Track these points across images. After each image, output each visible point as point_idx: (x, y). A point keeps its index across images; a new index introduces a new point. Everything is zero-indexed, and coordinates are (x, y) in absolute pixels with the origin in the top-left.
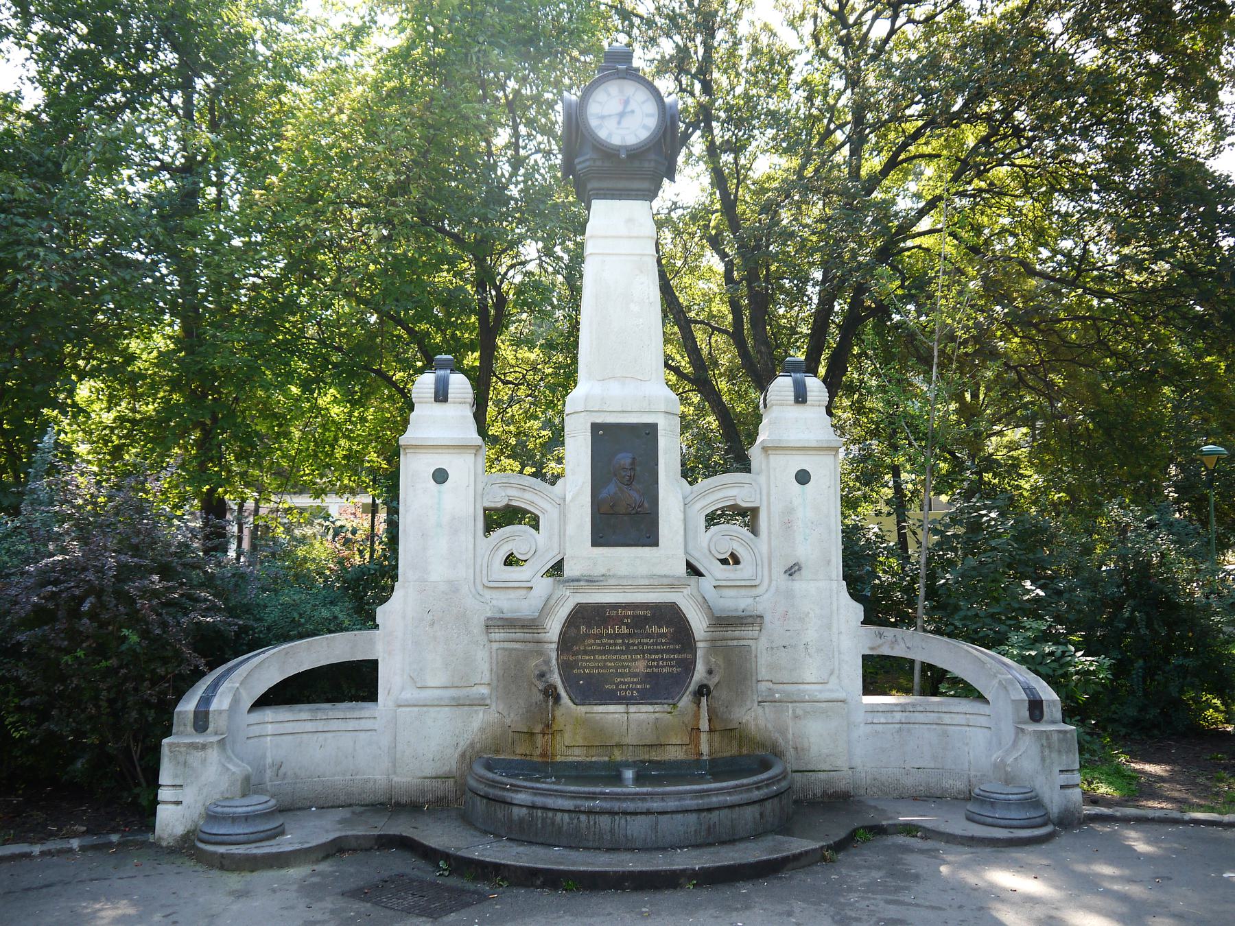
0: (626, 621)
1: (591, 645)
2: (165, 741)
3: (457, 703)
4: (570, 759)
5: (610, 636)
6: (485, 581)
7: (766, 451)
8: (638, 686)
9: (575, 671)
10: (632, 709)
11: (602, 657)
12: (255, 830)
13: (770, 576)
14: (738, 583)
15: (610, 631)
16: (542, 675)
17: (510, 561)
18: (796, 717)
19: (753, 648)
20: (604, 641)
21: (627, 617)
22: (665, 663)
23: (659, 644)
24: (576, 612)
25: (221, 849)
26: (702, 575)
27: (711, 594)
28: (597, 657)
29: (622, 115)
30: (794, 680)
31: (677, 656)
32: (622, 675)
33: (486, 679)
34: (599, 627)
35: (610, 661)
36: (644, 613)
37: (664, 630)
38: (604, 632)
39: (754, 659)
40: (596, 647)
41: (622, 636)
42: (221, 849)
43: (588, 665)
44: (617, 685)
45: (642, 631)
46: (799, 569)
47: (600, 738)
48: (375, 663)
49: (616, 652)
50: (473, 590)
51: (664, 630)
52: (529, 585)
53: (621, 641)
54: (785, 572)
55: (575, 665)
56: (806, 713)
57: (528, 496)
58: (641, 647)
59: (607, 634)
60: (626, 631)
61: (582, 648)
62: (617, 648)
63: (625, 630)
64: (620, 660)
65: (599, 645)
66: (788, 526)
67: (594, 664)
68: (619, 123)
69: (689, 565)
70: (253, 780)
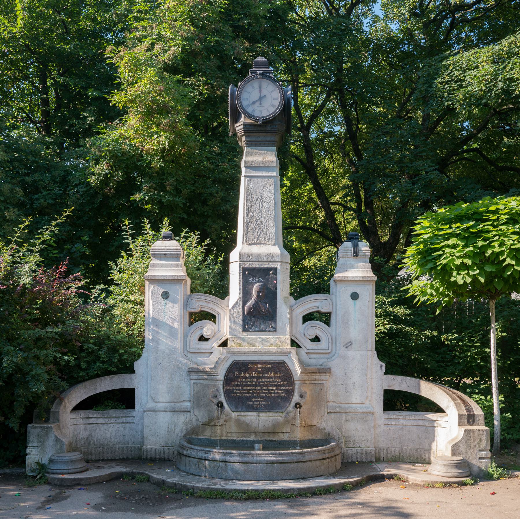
0: (258, 370)
1: (240, 382)
2: (29, 425)
3: (174, 411)
4: (230, 438)
5: (250, 377)
6: (188, 349)
7: (336, 282)
8: (264, 403)
9: (233, 395)
10: (261, 414)
11: (246, 388)
12: (74, 467)
13: (336, 348)
14: (319, 351)
15: (250, 375)
16: (216, 396)
17: (202, 339)
18: (347, 420)
19: (325, 385)
20: (247, 380)
21: (260, 368)
22: (278, 391)
23: (275, 382)
24: (233, 365)
25: (61, 476)
26: (300, 347)
27: (305, 357)
28: (243, 388)
29: (261, 99)
30: (346, 402)
31: (284, 388)
32: (256, 397)
33: (186, 397)
34: (245, 373)
35: (250, 390)
36: (268, 366)
37: (278, 375)
38: (247, 375)
39: (325, 390)
40: (243, 383)
41: (257, 378)
42: (61, 476)
43: (240, 392)
44: (254, 402)
45: (267, 375)
46: (351, 344)
47: (246, 429)
48: (133, 390)
49: (253, 386)
50: (183, 354)
51: (278, 375)
52: (211, 351)
53: (255, 380)
54: (344, 346)
55: (232, 391)
56: (353, 418)
57: (211, 305)
58: (266, 383)
59: (249, 376)
60: (259, 375)
61: (236, 383)
62: (254, 383)
63: (257, 374)
64: (255, 390)
65: (244, 382)
66: (346, 323)
67: (242, 391)
68: (261, 104)
69: (292, 341)
70: (74, 445)
